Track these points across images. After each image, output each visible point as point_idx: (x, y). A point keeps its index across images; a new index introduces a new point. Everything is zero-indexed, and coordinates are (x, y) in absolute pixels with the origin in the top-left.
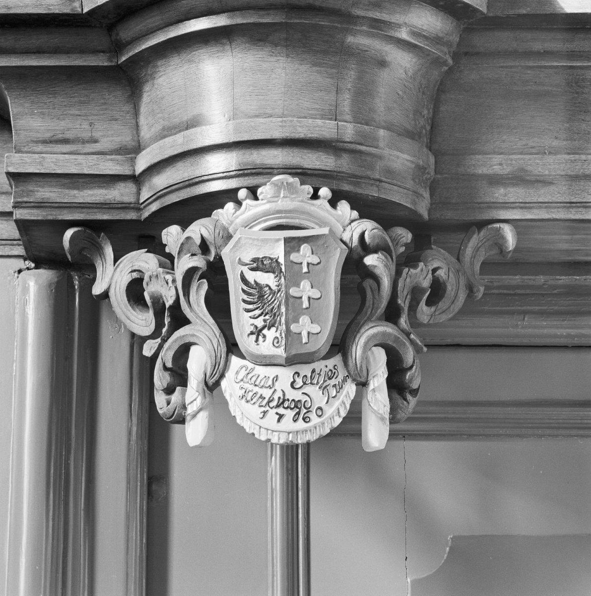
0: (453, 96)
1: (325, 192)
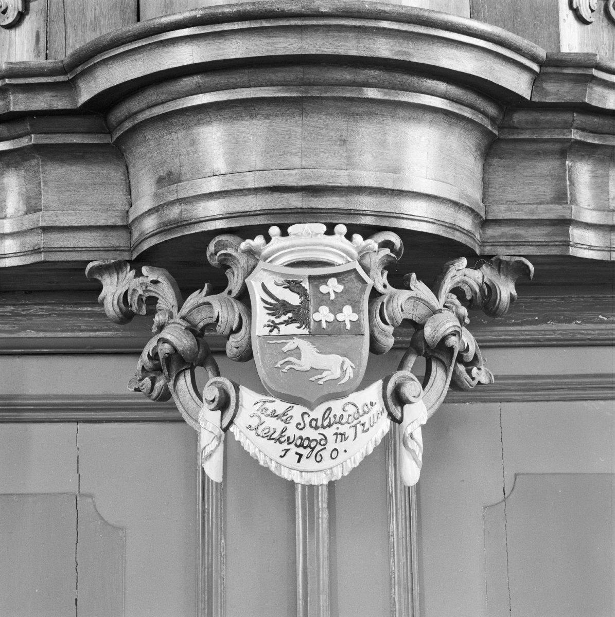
1: (341, 229)
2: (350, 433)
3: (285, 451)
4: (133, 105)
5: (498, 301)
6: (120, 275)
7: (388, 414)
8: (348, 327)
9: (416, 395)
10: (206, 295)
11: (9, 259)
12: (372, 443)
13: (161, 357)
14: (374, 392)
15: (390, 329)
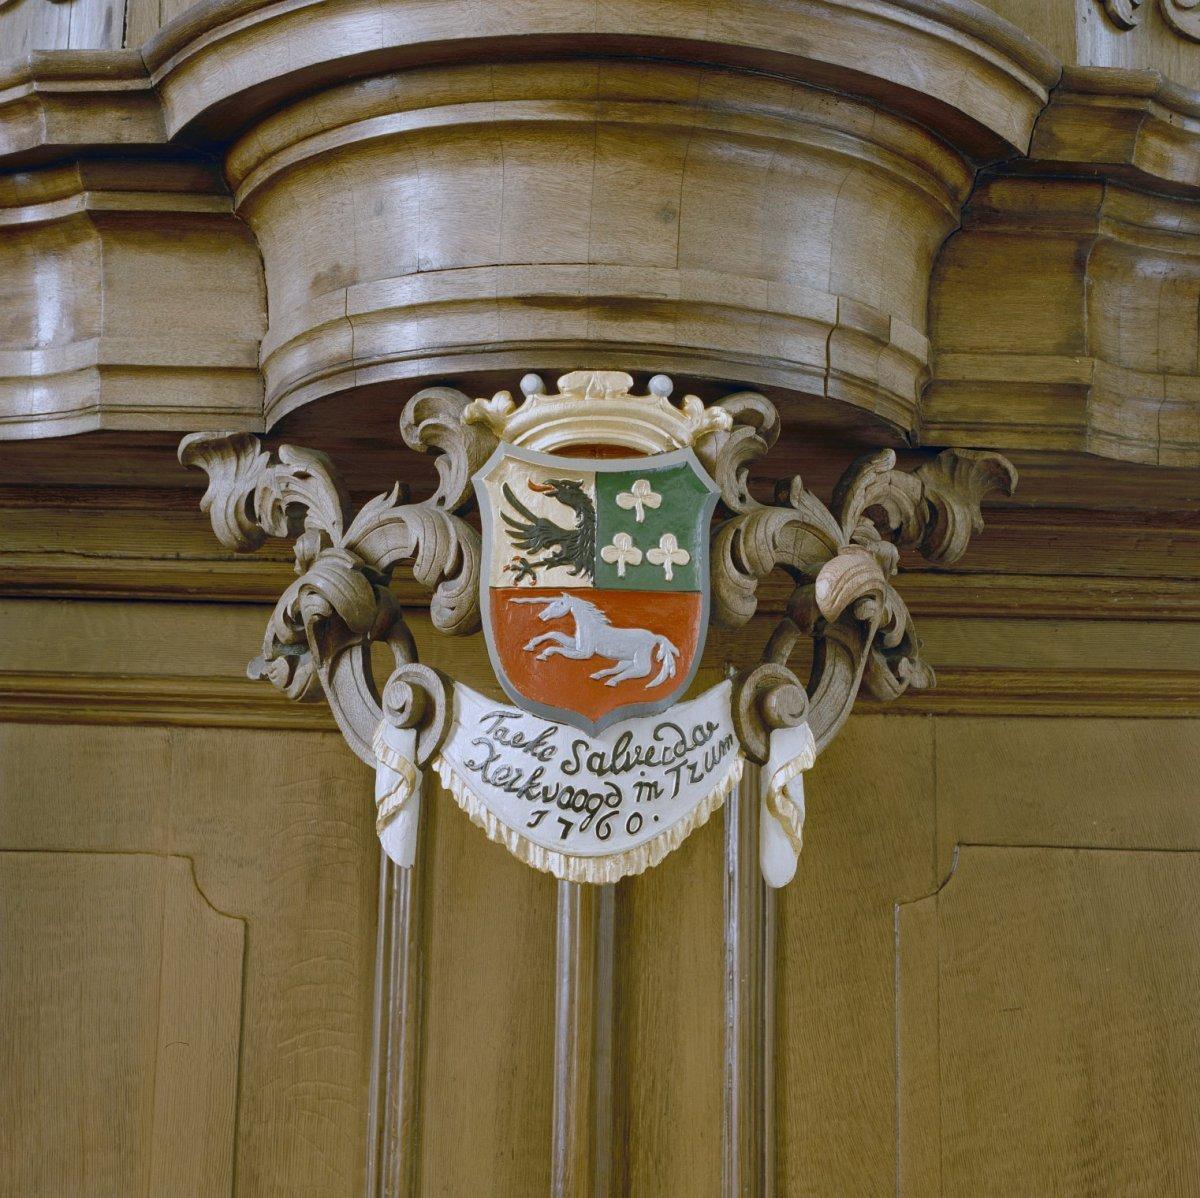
0: (1048, 342)
1: (660, 384)
2: (667, 782)
3: (538, 815)
4: (270, 136)
5: (949, 533)
6: (243, 460)
7: (741, 746)
8: (669, 576)
9: (796, 711)
10: (397, 504)
11: (39, 424)
12: (707, 803)
13: (306, 619)
14: (713, 705)
15: (752, 584)
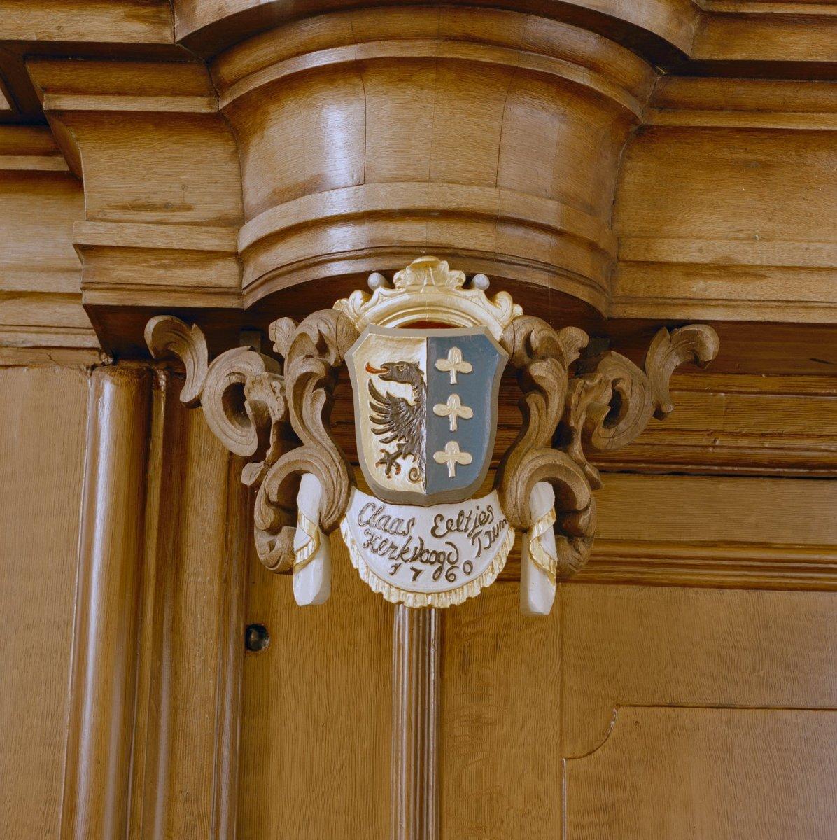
1: (481, 280)
3: (394, 568)
4: (264, 51)
